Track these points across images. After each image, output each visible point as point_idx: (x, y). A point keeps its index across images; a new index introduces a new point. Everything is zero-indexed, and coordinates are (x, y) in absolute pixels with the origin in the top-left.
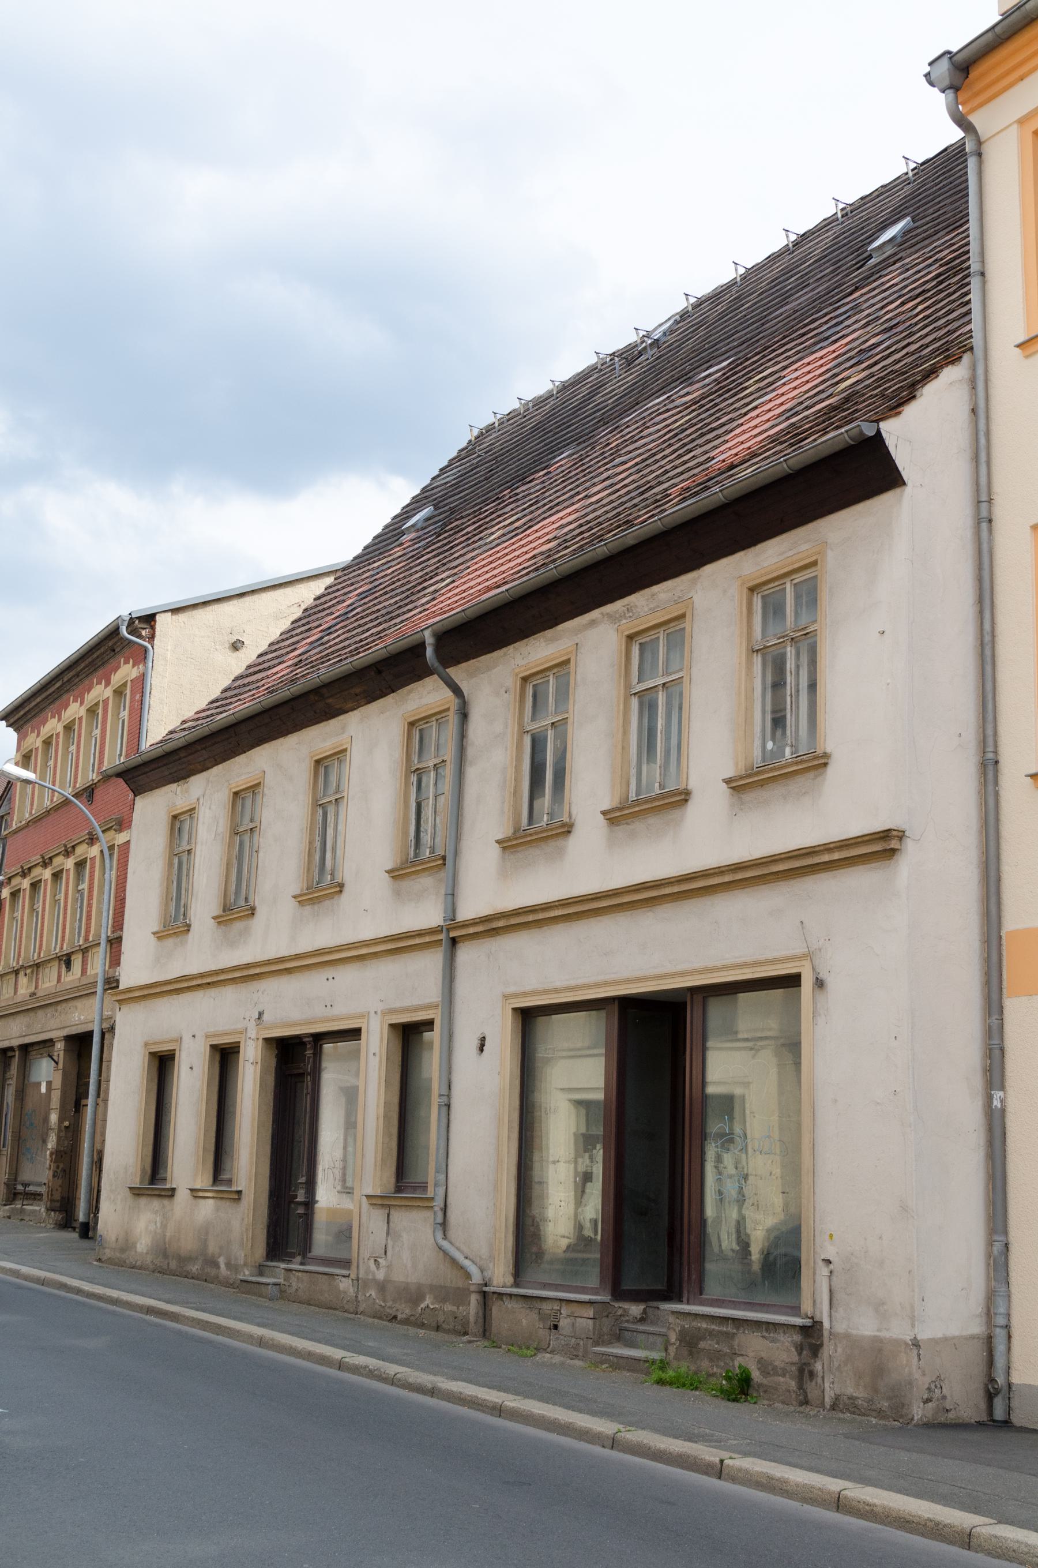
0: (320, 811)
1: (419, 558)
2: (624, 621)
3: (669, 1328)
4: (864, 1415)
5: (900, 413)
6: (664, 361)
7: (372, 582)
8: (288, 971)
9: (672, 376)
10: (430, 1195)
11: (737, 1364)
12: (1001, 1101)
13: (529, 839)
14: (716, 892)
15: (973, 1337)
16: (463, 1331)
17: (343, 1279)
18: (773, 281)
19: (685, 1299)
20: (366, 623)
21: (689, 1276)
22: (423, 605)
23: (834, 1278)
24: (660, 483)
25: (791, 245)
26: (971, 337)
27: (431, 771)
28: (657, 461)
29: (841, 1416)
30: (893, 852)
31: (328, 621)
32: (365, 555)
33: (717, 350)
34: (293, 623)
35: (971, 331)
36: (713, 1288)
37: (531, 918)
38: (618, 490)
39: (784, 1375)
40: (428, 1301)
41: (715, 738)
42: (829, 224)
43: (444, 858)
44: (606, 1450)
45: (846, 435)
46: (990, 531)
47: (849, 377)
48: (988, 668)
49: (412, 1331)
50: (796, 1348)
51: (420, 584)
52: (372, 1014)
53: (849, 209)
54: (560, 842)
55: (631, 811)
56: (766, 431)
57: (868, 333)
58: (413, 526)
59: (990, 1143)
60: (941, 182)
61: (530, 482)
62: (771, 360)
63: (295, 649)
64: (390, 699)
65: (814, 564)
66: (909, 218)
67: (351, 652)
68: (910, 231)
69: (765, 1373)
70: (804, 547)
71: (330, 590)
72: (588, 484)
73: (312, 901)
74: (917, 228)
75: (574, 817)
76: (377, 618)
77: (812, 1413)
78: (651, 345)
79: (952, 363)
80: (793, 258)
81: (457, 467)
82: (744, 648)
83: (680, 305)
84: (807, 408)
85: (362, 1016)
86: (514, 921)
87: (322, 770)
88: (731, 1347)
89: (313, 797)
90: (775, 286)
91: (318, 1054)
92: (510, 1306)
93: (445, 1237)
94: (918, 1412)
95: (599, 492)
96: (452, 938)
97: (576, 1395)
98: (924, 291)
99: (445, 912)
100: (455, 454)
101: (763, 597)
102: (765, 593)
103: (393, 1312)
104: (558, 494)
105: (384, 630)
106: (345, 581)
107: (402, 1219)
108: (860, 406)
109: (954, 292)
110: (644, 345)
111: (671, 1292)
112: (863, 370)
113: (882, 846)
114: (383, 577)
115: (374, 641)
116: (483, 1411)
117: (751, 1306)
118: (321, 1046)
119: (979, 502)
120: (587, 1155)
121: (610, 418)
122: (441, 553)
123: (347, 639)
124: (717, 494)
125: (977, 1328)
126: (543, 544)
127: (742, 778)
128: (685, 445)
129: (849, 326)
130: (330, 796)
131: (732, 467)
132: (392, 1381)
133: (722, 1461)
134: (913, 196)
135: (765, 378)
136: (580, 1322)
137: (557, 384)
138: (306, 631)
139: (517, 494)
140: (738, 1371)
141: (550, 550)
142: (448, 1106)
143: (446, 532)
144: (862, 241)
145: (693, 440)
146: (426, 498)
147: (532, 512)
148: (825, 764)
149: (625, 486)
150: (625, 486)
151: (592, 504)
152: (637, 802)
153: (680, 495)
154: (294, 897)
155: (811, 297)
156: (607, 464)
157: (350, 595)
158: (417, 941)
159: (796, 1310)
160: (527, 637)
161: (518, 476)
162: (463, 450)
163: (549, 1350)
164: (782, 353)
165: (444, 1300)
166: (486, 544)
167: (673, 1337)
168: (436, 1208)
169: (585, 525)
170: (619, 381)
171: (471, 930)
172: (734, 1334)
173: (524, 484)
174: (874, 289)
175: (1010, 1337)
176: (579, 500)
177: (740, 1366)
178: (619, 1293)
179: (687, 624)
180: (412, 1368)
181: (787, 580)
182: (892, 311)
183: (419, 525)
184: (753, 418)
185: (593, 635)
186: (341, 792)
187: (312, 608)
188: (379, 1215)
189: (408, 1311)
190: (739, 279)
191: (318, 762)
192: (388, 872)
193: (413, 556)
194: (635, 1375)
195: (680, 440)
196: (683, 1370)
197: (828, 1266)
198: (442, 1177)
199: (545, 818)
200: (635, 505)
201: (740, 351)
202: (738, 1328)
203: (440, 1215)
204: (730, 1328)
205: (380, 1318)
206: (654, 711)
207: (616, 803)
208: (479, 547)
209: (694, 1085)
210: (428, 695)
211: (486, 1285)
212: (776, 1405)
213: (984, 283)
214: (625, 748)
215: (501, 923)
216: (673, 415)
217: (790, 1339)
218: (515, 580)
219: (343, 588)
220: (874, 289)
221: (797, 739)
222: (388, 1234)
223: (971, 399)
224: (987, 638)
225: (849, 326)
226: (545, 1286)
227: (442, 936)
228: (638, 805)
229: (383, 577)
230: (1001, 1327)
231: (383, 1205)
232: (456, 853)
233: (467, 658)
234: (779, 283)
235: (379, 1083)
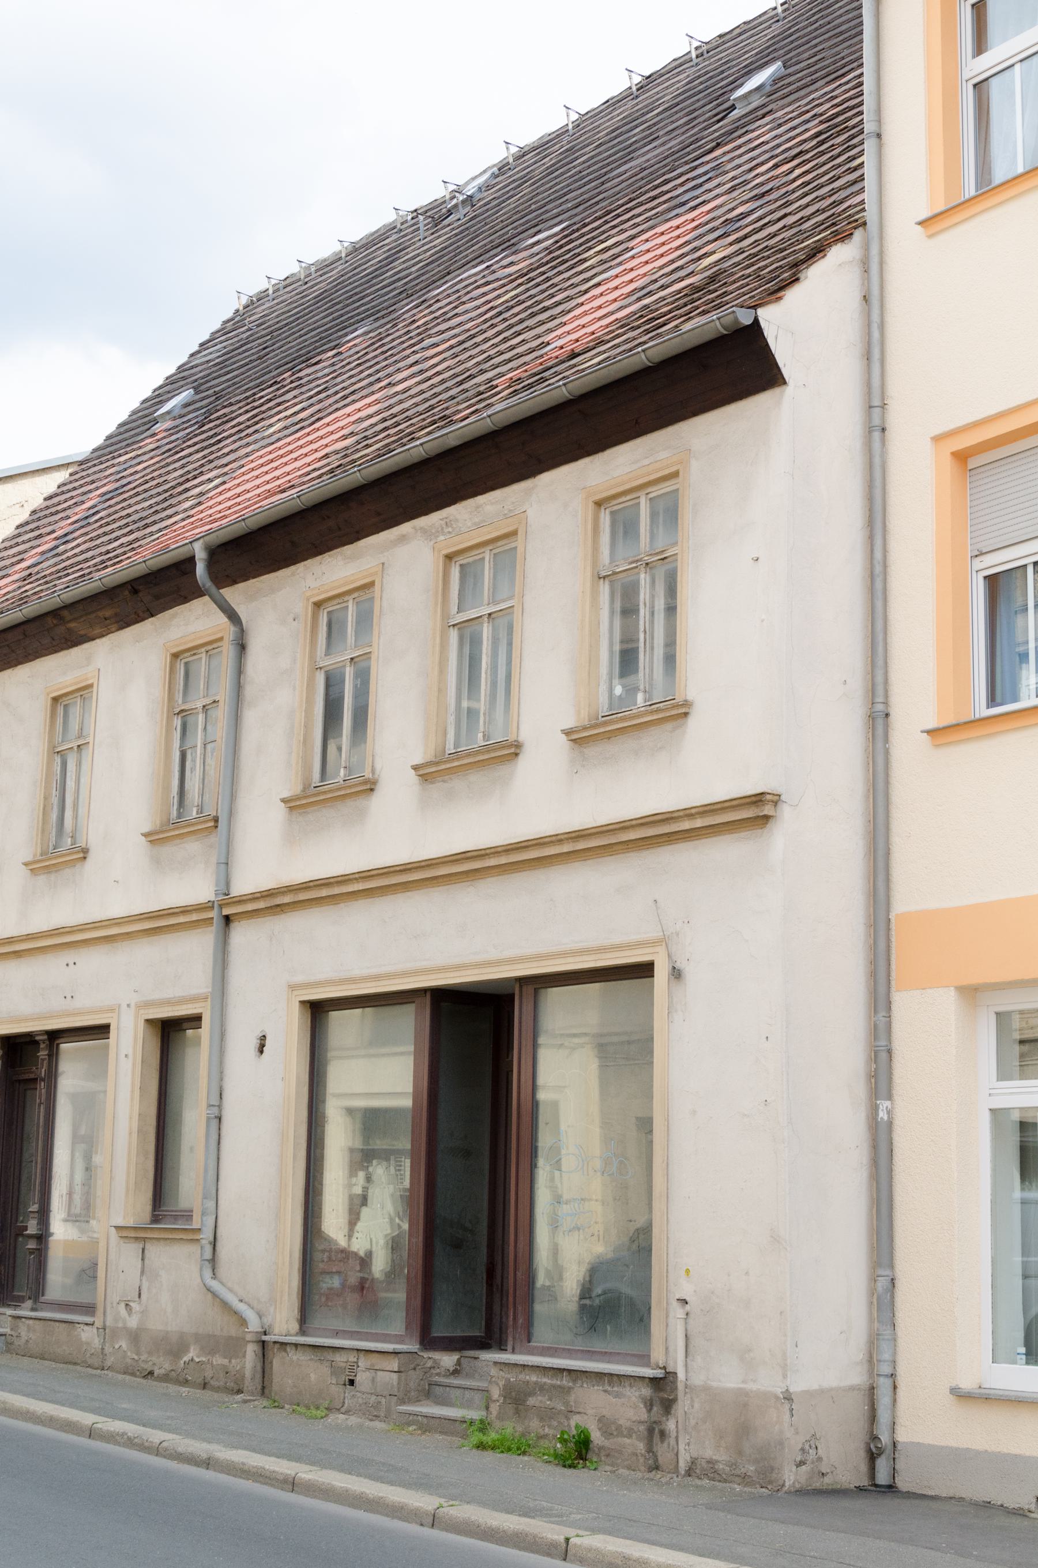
0: (58, 759)
1: (177, 453)
2: (442, 538)
3: (490, 1382)
4: (725, 1481)
5: (780, 298)
6: (479, 222)
7: (118, 480)
8: (17, 954)
9: (492, 241)
10: (195, 1225)
11: (573, 1423)
12: (888, 1112)
13: (322, 797)
14: (551, 864)
15: (852, 1388)
16: (236, 1388)
17: (86, 1328)
18: (613, 131)
19: (509, 1347)
20: (113, 531)
21: (515, 1319)
22: (186, 510)
23: (690, 1321)
24: (483, 372)
25: (634, 88)
26: (863, 210)
27: (195, 717)
28: (477, 345)
29: (699, 1482)
30: (766, 818)
31: (63, 527)
32: (108, 446)
33: (547, 212)
34: (18, 527)
35: (863, 202)
36: (543, 1334)
37: (324, 892)
38: (430, 379)
39: (630, 1436)
40: (193, 1353)
41: (552, 679)
42: (680, 65)
43: (216, 820)
44: (425, 1529)
45: (717, 322)
46: (883, 442)
47: (714, 252)
48: (879, 604)
49: (173, 1389)
50: (645, 1403)
51: (181, 484)
52: (124, 1007)
53: (705, 48)
54: (360, 802)
55: (448, 766)
56: (612, 313)
57: (735, 199)
58: (168, 413)
59: (875, 1162)
60: (816, 21)
61: (316, 364)
62: (614, 227)
63: (22, 560)
64: (149, 624)
65: (675, 475)
66: (779, 63)
67: (95, 565)
68: (781, 78)
69: (607, 1434)
70: (663, 455)
71: (65, 488)
72: (390, 370)
73: (48, 869)
74: (790, 75)
75: (377, 772)
76: (127, 525)
77: (664, 1480)
78: (463, 202)
79: (842, 240)
80: (637, 104)
81: (221, 342)
82: (589, 574)
83: (498, 155)
84: (663, 287)
85: (111, 1010)
86: (302, 896)
87: (60, 710)
88: (566, 1404)
89: (49, 742)
90: (616, 137)
91: (54, 1055)
92: (295, 1358)
93: (214, 1276)
94: (790, 1476)
95: (405, 380)
96: (226, 916)
97: (384, 1464)
98: (801, 152)
99: (217, 885)
100: (217, 326)
101: (612, 513)
102: (616, 510)
103: (148, 1367)
104: (353, 380)
105: (137, 540)
106: (83, 477)
107: (160, 1255)
108: (731, 288)
109: (839, 155)
110: (455, 201)
111: (491, 1338)
112: (731, 244)
113: (754, 812)
114: (131, 475)
115: (125, 553)
116: (272, 1485)
117: (590, 1355)
118: (58, 1045)
119: (870, 407)
120: (361, 1175)
121: (416, 288)
122: (206, 448)
123: (89, 550)
124: (558, 389)
125: (857, 1377)
126: (337, 441)
127: (585, 728)
128: (511, 326)
129: (710, 190)
130: (70, 741)
131: (574, 355)
132: (157, 1451)
133: (567, 1540)
134: (784, 35)
135: (608, 249)
136: (379, 1377)
137: (346, 244)
138: (36, 538)
139: (301, 378)
140: (574, 1432)
141: (346, 448)
142: (220, 1119)
143: (211, 421)
144: (721, 88)
145: (522, 321)
146: (184, 378)
147: (321, 401)
148: (686, 714)
149: (438, 373)
150: (438, 373)
151: (397, 393)
152: (456, 755)
153: (510, 387)
154: (26, 864)
155: (662, 153)
156: (413, 345)
157: (91, 495)
158: (182, 919)
159: (644, 1359)
160: (321, 553)
161: (301, 356)
162: (228, 321)
163: (343, 1410)
164: (628, 220)
165: (212, 1352)
166: (263, 438)
167: (496, 1393)
168: (203, 1242)
169: (389, 420)
170: (423, 245)
171: (250, 907)
172: (570, 1388)
173: (308, 366)
174: (740, 147)
175: (895, 1387)
176: (381, 389)
177: (577, 1426)
178: (429, 1341)
179: (519, 542)
180: (179, 1434)
181: (642, 494)
182: (762, 174)
183: (176, 413)
184: (595, 297)
185: (403, 552)
186: (85, 737)
187: (41, 510)
188: (132, 1250)
189: (167, 1366)
190: (570, 127)
191: (56, 700)
192: (145, 835)
193: (170, 450)
194: (449, 1438)
195: (505, 320)
196: (509, 1431)
197: (683, 1307)
198: (211, 1204)
199: (342, 772)
200: (453, 398)
201: (576, 215)
202: (575, 1381)
203: (208, 1249)
204: (565, 1382)
205: (133, 1374)
206: (478, 646)
207: (430, 757)
208: (255, 442)
209: (523, 1091)
210: (194, 621)
211: (265, 1333)
212: (621, 1471)
213: (880, 147)
214: (441, 691)
215: (287, 899)
216: (495, 289)
217: (637, 1394)
218: (304, 483)
219: (81, 486)
220: (740, 147)
221: (651, 685)
222: (143, 1272)
223: (863, 284)
224: (878, 569)
225: (710, 190)
226: (337, 1334)
227: (214, 914)
228: (458, 759)
229: (131, 475)
230: (887, 1376)
231: (136, 1238)
232: (231, 814)
233: (245, 578)
234: (621, 134)
235: (132, 1091)
